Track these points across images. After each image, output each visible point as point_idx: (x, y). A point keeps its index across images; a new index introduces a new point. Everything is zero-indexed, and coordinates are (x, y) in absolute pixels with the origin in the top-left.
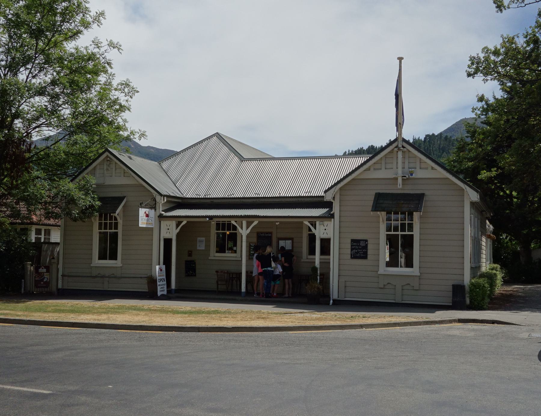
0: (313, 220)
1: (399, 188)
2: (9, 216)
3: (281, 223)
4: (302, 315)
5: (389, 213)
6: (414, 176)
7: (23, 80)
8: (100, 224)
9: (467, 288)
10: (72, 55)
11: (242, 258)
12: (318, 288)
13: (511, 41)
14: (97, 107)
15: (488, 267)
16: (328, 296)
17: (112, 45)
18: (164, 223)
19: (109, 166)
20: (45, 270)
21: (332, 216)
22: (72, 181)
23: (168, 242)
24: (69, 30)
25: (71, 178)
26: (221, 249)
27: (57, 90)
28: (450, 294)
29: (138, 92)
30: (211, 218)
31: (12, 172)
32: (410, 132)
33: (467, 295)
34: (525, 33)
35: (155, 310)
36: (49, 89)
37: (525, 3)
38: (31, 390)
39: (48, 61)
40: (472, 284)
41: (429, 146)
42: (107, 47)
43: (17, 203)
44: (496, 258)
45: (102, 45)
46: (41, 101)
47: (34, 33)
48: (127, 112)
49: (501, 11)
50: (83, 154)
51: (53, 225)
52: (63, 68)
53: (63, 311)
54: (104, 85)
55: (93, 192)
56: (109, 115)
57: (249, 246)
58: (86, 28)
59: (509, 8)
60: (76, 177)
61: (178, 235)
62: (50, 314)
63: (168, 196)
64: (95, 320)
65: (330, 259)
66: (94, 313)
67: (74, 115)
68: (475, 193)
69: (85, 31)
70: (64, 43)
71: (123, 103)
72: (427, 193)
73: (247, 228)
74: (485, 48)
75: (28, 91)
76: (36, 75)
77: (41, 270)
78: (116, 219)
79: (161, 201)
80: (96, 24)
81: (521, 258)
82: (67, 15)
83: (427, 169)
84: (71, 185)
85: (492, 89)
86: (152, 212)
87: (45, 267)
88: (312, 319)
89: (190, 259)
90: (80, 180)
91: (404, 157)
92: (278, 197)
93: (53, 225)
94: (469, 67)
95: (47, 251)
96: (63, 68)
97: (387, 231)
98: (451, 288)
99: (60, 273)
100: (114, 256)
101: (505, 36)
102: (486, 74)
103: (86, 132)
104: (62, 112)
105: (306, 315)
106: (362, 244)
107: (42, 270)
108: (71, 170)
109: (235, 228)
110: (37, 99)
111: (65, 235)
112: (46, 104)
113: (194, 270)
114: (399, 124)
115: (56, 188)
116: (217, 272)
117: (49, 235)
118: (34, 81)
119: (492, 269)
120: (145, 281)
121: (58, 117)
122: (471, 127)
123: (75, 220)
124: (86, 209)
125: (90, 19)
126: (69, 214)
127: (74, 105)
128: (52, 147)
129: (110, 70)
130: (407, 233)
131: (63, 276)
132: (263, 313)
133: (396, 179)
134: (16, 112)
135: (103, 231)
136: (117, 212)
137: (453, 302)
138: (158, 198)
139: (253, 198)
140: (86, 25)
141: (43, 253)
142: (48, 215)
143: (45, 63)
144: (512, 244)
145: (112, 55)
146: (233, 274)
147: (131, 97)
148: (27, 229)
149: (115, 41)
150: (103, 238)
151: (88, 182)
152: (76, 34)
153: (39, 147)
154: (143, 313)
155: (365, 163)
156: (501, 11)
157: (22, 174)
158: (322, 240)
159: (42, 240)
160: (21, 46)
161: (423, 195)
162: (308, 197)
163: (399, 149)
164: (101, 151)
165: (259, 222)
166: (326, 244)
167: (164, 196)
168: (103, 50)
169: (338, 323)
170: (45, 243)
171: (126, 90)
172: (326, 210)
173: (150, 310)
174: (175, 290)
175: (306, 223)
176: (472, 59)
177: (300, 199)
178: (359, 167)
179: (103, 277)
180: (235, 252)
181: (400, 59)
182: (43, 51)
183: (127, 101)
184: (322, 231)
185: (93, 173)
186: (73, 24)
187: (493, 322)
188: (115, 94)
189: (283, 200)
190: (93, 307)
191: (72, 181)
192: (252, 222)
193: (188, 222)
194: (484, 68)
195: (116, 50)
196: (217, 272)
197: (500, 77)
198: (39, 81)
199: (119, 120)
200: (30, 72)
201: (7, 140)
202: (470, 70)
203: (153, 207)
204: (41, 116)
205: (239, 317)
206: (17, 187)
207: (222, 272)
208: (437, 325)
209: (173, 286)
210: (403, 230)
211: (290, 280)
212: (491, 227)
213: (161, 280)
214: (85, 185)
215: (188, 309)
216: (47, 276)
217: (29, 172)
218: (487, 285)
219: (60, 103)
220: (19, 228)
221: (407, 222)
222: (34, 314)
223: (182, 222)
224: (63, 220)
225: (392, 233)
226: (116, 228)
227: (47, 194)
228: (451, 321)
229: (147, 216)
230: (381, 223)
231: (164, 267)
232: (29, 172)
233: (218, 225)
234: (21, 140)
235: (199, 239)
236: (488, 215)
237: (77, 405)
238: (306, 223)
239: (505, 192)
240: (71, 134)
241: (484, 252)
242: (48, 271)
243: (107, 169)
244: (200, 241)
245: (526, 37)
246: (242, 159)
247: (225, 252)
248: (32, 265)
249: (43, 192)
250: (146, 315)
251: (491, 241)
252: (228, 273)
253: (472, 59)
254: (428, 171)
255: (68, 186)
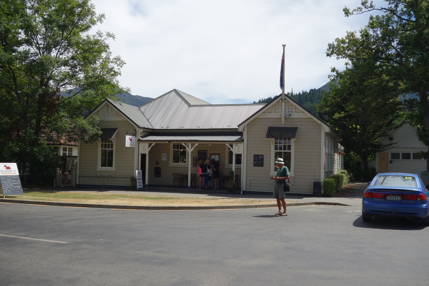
0: (231, 143)
1: (283, 124)
2: (46, 140)
3: (212, 144)
4: (222, 200)
5: (276, 139)
6: (291, 117)
7: (54, 56)
8: (102, 145)
9: (322, 184)
10: (84, 40)
11: (188, 166)
12: (234, 184)
13: (352, 34)
14: (100, 73)
15: (340, 172)
16: (240, 189)
17: (109, 35)
18: (141, 145)
19: (107, 109)
20: (68, 173)
21: (243, 141)
22: (84, 119)
23: (143, 156)
24: (83, 25)
25: (84, 117)
26: (176, 159)
27: (75, 62)
28: (312, 188)
29: (125, 64)
30: (170, 141)
31: (48, 113)
32: (287, 90)
33: (322, 188)
34: (361, 30)
35: (134, 197)
36: (70, 62)
37: (362, 11)
38: (55, 242)
39: (70, 45)
40: (325, 182)
41: (303, 100)
42: (106, 36)
43: (51, 132)
44: (346, 165)
45: (103, 35)
46: (65, 69)
47: (61, 28)
48: (119, 76)
49: (348, 16)
50: (91, 102)
51: (74, 145)
52: (79, 49)
53: (78, 198)
54: (106, 58)
55: (98, 125)
56: (107, 77)
57: (193, 159)
58: (93, 24)
59: (352, 14)
60: (88, 116)
61: (150, 152)
62: (70, 199)
63: (144, 128)
64: (97, 202)
66: (96, 199)
67: (86, 78)
68: (327, 127)
69: (92, 26)
70: (80, 33)
71: (116, 70)
72: (299, 127)
73: (192, 147)
74: (337, 39)
75: (57, 63)
76: (62, 53)
77: (66, 173)
78: (112, 142)
79: (139, 131)
80: (99, 22)
81: (362, 166)
82: (81, 16)
83: (299, 112)
84: (84, 121)
85: (342, 64)
86: (134, 138)
87: (69, 171)
88: (228, 202)
89: (157, 166)
90: (90, 118)
91: (286, 105)
92: (210, 129)
93: (74, 145)
94: (328, 50)
95: (69, 161)
96: (79, 49)
97: (275, 150)
98: (312, 184)
99: (78, 175)
100: (110, 165)
101: (349, 32)
102: (338, 55)
103: (94, 88)
104: (79, 76)
105: (225, 200)
106: (260, 157)
107: (67, 173)
108: (85, 111)
109: (185, 148)
110: (63, 68)
111: (80, 152)
112: (69, 71)
113: (160, 173)
114: (282, 85)
115: (75, 123)
116: (174, 174)
117: (72, 151)
118: (61, 56)
119: (342, 173)
120: (129, 180)
121: (76, 79)
122: (332, 86)
123: (86, 142)
124: (93, 136)
125: (95, 19)
126: (83, 139)
127: (86, 72)
128: (73, 97)
129: (108, 50)
130: (287, 151)
131: (79, 176)
132: (200, 199)
133: (281, 118)
134: (50, 76)
135: (104, 149)
136: (113, 137)
137: (314, 192)
138: (137, 129)
139: (196, 129)
140: (93, 23)
141: (67, 163)
142: (70, 139)
143: (68, 46)
144: (357, 158)
145: (108, 41)
146: (183, 175)
147: (121, 67)
148: (58, 148)
149: (111, 33)
150: (104, 153)
151: (94, 119)
152: (87, 28)
153: (65, 97)
154: (127, 199)
155: (262, 109)
156: (348, 16)
157: (54, 114)
159: (67, 154)
160: (53, 35)
161: (297, 128)
162: (229, 129)
163: (283, 100)
164: (103, 100)
165: (199, 144)
166: (239, 157)
167: (141, 128)
168: (103, 38)
169: (243, 205)
170: (68, 156)
171: (118, 62)
172: (239, 137)
173: (131, 197)
174: (148, 185)
175: (227, 145)
176: (330, 45)
177: (224, 130)
178: (259, 111)
179: (104, 177)
180: (185, 162)
181: (284, 46)
182: (66, 38)
183: (119, 69)
184: (237, 150)
185: (98, 114)
186: (85, 22)
187: (335, 204)
188: (111, 65)
189: (214, 131)
190: (97, 195)
191: (84, 119)
192: (195, 144)
193: (156, 144)
194: (337, 51)
195: (112, 38)
196: (174, 174)
197: (350, 56)
198: (64, 56)
199: (114, 81)
200: (59, 51)
201: (44, 93)
202: (328, 52)
203: (135, 135)
204: (66, 78)
205: (185, 201)
206: (51, 122)
207: (176, 174)
208: (302, 206)
209: (147, 182)
210: (285, 149)
211: (218, 179)
212: (343, 148)
213: (139, 179)
214: (92, 121)
215: (155, 196)
216: (69, 176)
217: (58, 113)
218: (334, 182)
219: (77, 70)
220: (53, 147)
221: (287, 144)
222: (60, 199)
223: (152, 144)
224: (79, 142)
225: (278, 151)
226: (112, 147)
227: (69, 126)
228: (310, 204)
229: (131, 140)
230: (272, 145)
231: (141, 171)
232: (58, 113)
233: (174, 145)
234: (54, 93)
235: (163, 154)
236: (339, 140)
237: (81, 249)
238: (227, 145)
239: (352, 126)
240: (84, 90)
241: (336, 162)
242: (70, 174)
243: (106, 112)
244: (164, 156)
245: (361, 33)
246: (190, 105)
247: (178, 162)
248: (60, 170)
249: (66, 125)
250: (128, 200)
251: (343, 156)
252: (180, 175)
253: (330, 45)
254: (300, 114)
255: (83, 122)
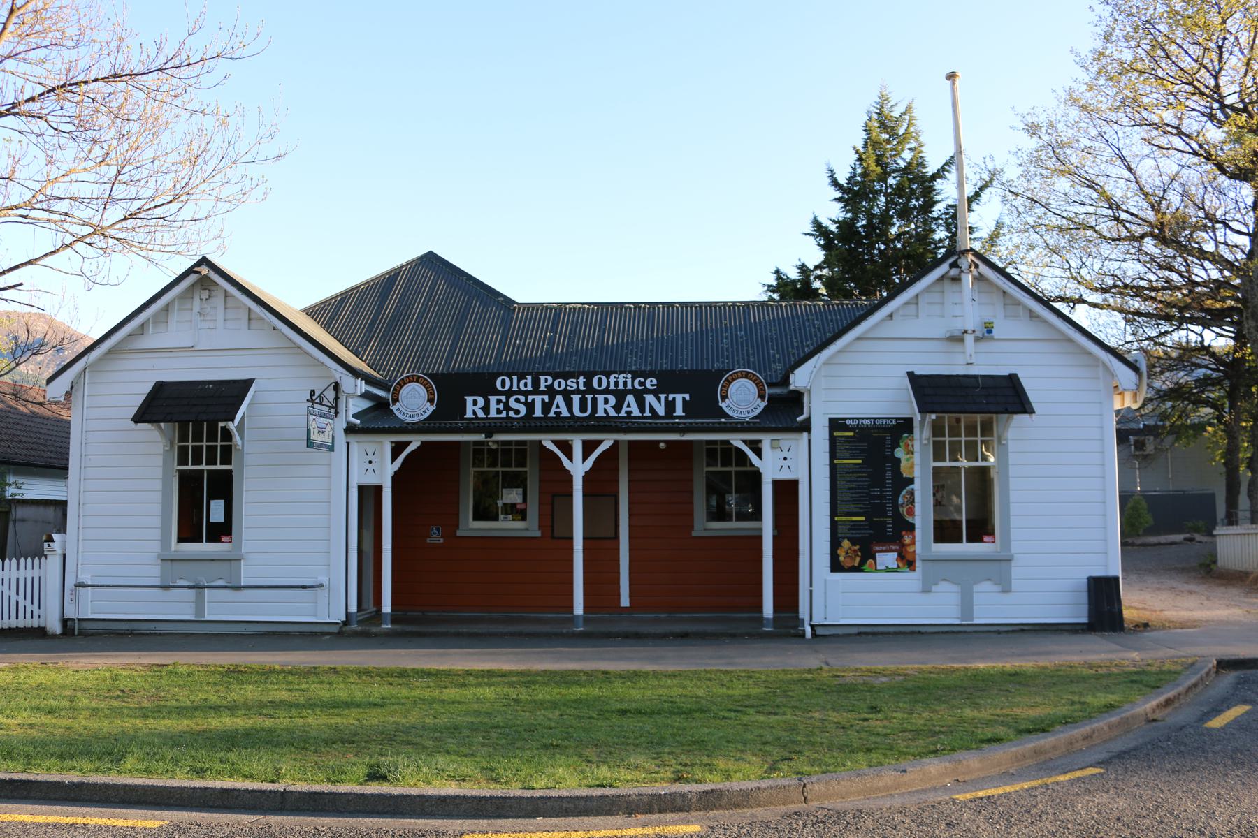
23: (370, 496)
61: (396, 478)
65: (761, 529)
73: (585, 458)
97: (179, 464)
158: (777, 484)
166: (787, 491)
181: (951, 76)
223: (407, 444)
